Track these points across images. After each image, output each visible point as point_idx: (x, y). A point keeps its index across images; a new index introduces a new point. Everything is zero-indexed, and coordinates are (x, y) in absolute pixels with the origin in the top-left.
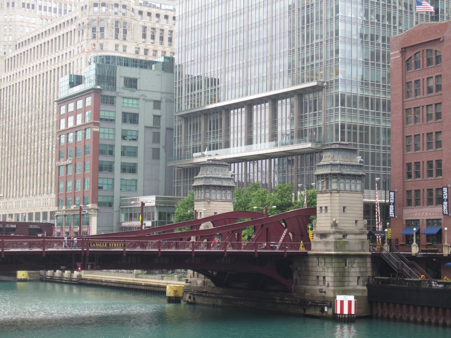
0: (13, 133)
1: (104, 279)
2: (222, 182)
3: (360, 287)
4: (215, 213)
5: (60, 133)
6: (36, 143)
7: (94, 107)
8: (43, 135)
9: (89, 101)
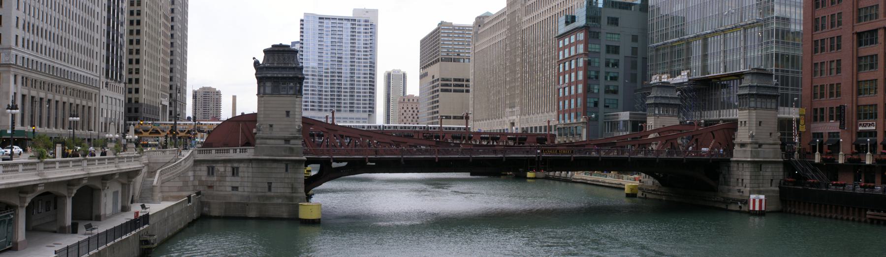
0: (532, 64)
1: (600, 180)
2: (669, 101)
3: (773, 188)
5: (559, 62)
6: (548, 71)
8: (553, 65)
9: (581, 36)
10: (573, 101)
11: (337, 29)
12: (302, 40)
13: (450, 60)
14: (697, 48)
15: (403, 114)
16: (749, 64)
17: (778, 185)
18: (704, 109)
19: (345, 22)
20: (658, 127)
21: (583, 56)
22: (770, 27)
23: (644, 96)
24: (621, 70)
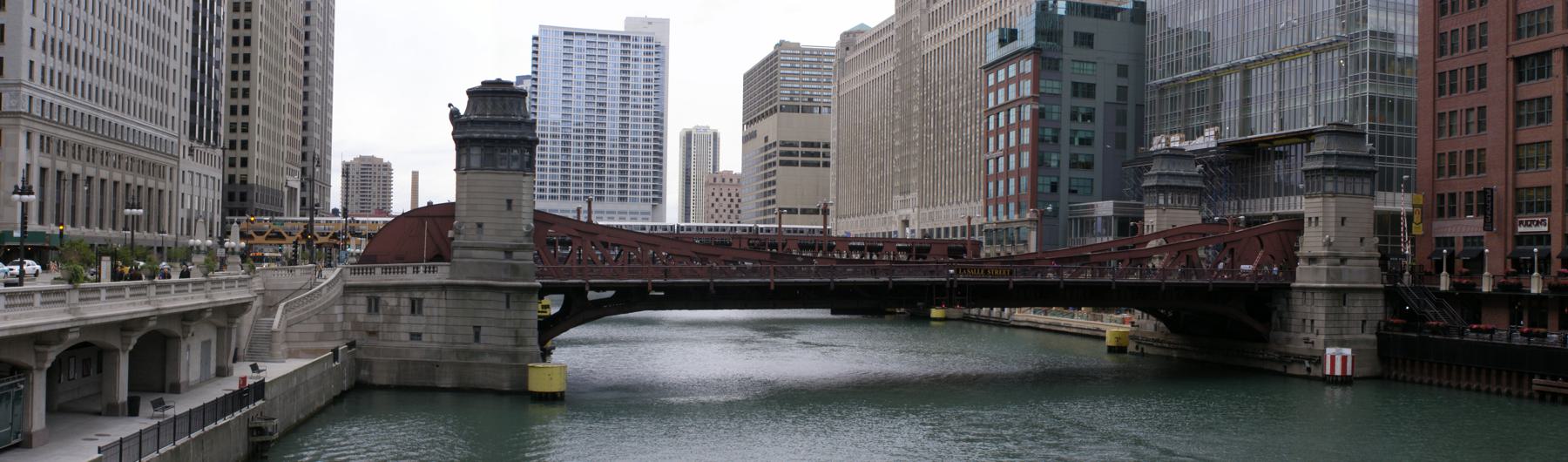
1: (1062, 323)
4: (1174, 226)
6: (969, 128)
8: (978, 117)
9: (1027, 65)
10: (1012, 182)
11: (597, 53)
12: (536, 73)
13: (795, 109)
14: (1231, 87)
15: (713, 205)
16: (1322, 115)
17: (1375, 331)
18: (1245, 195)
19: (610, 41)
20: (1164, 228)
21: (1031, 100)
22: (1359, 50)
23: (1140, 174)
24: (1098, 128)
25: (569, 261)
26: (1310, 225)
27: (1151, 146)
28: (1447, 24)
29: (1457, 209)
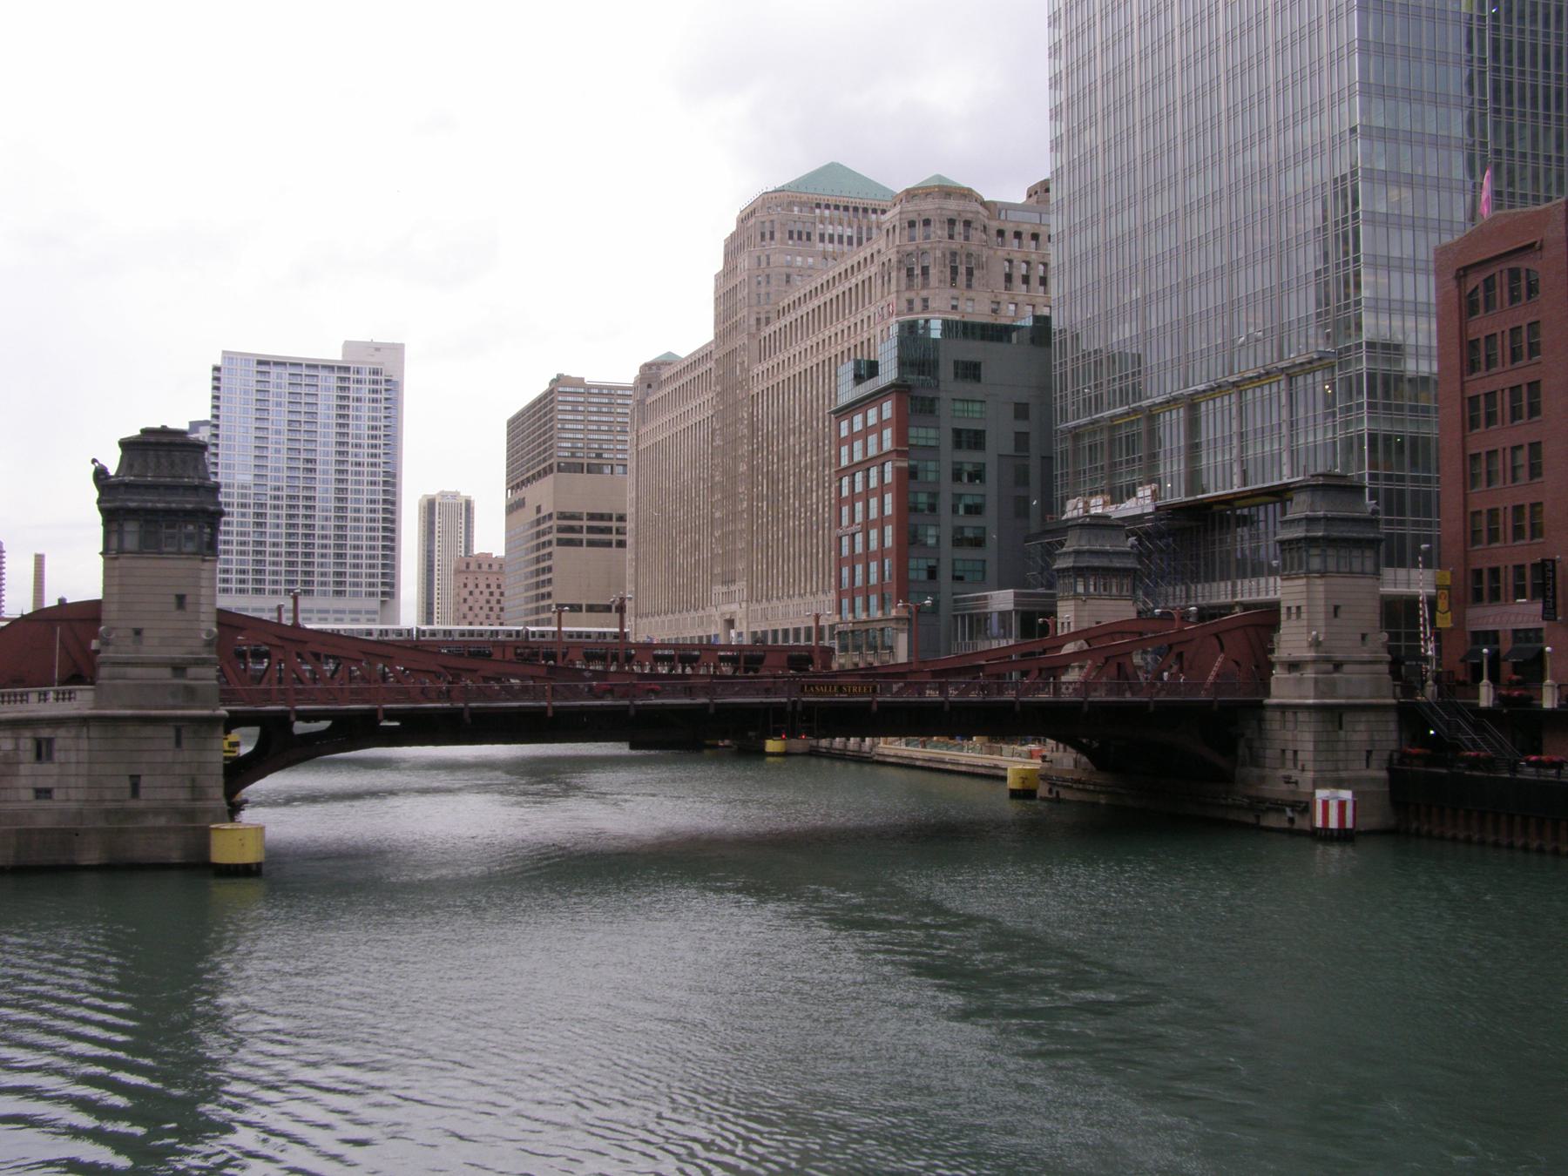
1: (947, 758)
5: (841, 473)
7: (898, 422)
9: (888, 409)
10: (874, 566)
11: (304, 390)
12: (216, 417)
13: (576, 468)
14: (1172, 427)
15: (465, 600)
16: (1302, 463)
17: (1385, 766)
18: (1196, 578)
19: (322, 373)
20: (1085, 625)
21: (894, 456)
22: (1352, 370)
23: (1050, 552)
24: (989, 490)
25: (265, 680)
26: (1289, 617)
27: (1063, 513)
28: (1481, 326)
29: (1502, 591)
